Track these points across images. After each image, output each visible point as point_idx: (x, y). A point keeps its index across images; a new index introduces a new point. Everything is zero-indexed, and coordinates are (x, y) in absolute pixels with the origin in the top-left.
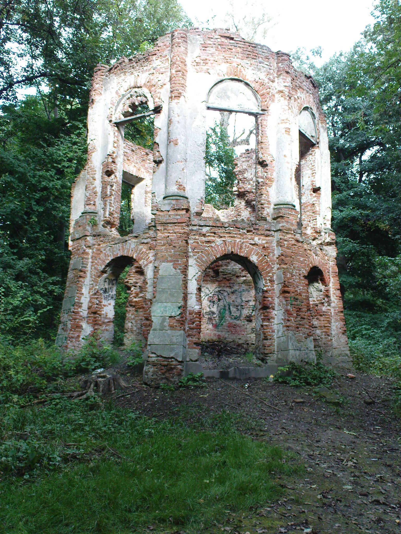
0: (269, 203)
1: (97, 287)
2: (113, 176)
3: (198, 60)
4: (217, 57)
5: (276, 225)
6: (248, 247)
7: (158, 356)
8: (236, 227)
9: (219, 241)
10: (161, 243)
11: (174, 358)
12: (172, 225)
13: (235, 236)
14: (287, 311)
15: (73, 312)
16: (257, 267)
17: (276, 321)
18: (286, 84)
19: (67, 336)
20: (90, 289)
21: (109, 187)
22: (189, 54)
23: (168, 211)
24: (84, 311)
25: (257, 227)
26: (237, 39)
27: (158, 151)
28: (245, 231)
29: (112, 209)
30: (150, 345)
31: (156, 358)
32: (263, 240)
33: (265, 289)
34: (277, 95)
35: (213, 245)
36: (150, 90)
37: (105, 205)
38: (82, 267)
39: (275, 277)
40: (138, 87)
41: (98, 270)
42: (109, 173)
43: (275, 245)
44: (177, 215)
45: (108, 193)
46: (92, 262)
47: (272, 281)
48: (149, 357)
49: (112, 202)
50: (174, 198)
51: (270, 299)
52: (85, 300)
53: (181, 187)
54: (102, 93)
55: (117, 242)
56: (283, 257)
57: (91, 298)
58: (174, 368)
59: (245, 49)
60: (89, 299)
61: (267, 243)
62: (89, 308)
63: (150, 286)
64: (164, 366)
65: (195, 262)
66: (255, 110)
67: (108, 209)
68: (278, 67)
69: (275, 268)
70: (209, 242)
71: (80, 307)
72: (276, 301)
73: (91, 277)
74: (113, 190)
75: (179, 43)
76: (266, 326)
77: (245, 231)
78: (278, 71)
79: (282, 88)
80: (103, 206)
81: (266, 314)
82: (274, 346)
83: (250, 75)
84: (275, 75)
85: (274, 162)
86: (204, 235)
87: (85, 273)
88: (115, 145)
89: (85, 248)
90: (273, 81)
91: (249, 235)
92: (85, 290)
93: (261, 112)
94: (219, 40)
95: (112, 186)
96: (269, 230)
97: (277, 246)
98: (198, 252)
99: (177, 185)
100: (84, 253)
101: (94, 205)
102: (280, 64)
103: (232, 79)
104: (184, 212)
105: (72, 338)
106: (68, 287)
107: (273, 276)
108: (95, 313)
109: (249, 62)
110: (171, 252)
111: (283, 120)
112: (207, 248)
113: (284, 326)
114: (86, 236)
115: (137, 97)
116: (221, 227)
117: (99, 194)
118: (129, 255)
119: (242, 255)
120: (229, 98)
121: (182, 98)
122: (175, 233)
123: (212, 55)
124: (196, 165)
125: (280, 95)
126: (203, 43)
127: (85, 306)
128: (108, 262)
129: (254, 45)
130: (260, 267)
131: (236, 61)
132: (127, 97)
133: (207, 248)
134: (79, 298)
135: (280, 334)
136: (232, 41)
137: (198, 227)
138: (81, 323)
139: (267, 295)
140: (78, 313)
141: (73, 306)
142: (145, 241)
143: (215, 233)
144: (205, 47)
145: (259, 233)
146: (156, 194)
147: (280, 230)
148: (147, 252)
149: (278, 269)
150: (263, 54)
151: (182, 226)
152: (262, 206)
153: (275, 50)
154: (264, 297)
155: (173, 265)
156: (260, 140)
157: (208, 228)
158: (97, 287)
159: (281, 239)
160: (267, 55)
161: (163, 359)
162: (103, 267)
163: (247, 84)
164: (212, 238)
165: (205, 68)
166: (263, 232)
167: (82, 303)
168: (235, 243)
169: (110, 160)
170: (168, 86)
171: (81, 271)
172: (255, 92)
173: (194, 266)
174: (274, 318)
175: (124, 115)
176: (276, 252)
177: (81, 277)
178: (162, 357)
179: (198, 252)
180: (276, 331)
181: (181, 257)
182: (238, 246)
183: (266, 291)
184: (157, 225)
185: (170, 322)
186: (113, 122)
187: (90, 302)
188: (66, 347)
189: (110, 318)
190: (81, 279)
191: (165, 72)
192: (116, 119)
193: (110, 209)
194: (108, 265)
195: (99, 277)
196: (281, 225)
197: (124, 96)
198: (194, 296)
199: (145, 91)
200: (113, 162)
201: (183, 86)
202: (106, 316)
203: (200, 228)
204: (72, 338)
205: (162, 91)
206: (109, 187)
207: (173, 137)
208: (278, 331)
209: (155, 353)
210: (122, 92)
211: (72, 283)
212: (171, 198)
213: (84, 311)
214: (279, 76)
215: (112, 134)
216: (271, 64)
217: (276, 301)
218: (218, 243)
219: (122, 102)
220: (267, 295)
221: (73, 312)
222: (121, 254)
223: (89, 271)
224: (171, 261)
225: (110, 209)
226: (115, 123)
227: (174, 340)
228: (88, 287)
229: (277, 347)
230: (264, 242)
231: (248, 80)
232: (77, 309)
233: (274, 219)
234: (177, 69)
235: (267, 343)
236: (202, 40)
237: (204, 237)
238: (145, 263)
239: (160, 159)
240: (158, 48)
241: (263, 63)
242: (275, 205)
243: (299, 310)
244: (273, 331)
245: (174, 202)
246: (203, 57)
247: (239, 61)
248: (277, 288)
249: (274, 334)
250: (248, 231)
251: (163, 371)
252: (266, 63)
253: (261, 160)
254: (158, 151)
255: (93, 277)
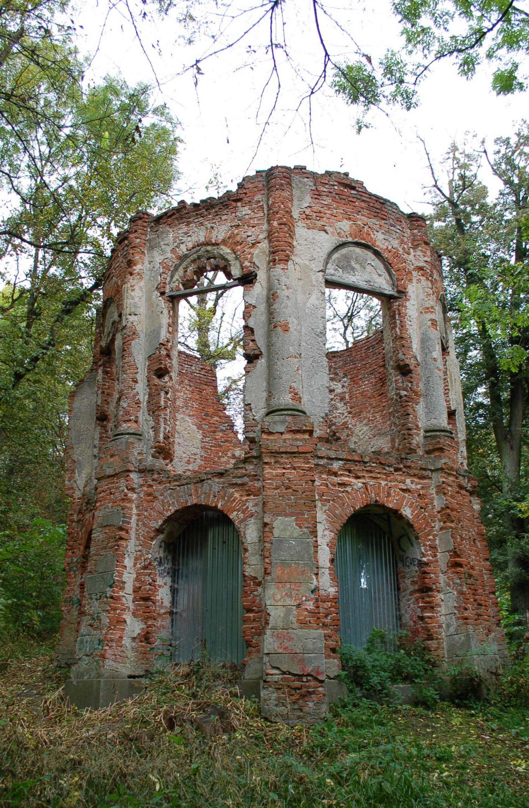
0: (418, 428)
1: (150, 556)
2: (167, 378)
3: (308, 211)
4: (335, 211)
5: (434, 461)
6: (398, 495)
7: (284, 673)
8: (380, 463)
9: (358, 484)
10: (272, 484)
11: (312, 676)
12: (288, 455)
13: (379, 476)
14: (461, 593)
15: (112, 597)
16: (411, 526)
17: (443, 610)
18: (426, 259)
19: (102, 637)
20: (136, 559)
21: (163, 394)
22: (295, 202)
23: (282, 434)
24: (127, 596)
25: (408, 464)
26: (360, 190)
27: (253, 341)
28: (392, 469)
29: (168, 429)
30: (268, 654)
31: (280, 676)
32: (417, 484)
33: (425, 559)
34: (415, 273)
35: (349, 489)
36: (233, 250)
37: (158, 423)
38: (124, 522)
39: (437, 542)
40: (213, 245)
41: (150, 528)
42: (161, 373)
43: (434, 492)
44: (297, 440)
45: (162, 403)
46: (138, 515)
47: (433, 548)
48: (267, 674)
49: (168, 418)
50: (290, 412)
51: (432, 575)
52: (129, 578)
53: (297, 397)
54: (146, 252)
55: (184, 482)
56: (448, 511)
57: (138, 574)
58: (314, 692)
59: (372, 205)
60: (135, 576)
61: (423, 488)
62: (136, 590)
63: (252, 555)
64: (296, 689)
65: (325, 516)
66: (388, 290)
67: (162, 429)
68: (413, 234)
69: (437, 528)
70: (340, 485)
71: (123, 588)
72: (441, 578)
73: (138, 539)
74: (168, 399)
75: (282, 185)
76: (430, 617)
77: (392, 469)
78: (414, 240)
79: (422, 264)
80: (152, 423)
81: (428, 599)
82: (443, 648)
83: (380, 240)
84: (410, 245)
85: (419, 368)
86: (335, 474)
87: (127, 532)
88: (171, 329)
89: (126, 491)
90: (409, 254)
91: (398, 476)
92: (128, 562)
93: (396, 294)
94: (336, 187)
95: (167, 393)
96: (425, 469)
97: (437, 493)
98: (328, 501)
99: (290, 393)
100: (126, 499)
101: (136, 422)
102: (415, 231)
103: (358, 244)
104: (307, 436)
105: (112, 640)
106: (95, 555)
107: (435, 540)
108: (146, 599)
109: (377, 223)
110: (289, 499)
111: (428, 308)
112: (340, 495)
113: (458, 618)
114: (129, 471)
115: (209, 259)
116: (359, 462)
117: (144, 405)
118: (209, 503)
119: (390, 506)
120: (353, 269)
121: (290, 263)
122: (294, 468)
123: (328, 206)
124: (315, 364)
125: (420, 274)
126: (314, 188)
127: (129, 588)
128: (169, 514)
129: (382, 201)
130: (416, 525)
131: (362, 219)
132: (192, 258)
133: (340, 495)
134: (121, 575)
135: (452, 630)
136: (353, 192)
137: (326, 461)
138: (124, 616)
139: (427, 569)
140: (118, 599)
141: (111, 587)
142: (239, 481)
143: (350, 471)
144: (317, 195)
145: (411, 472)
146: (252, 406)
147: (442, 469)
148: (244, 499)
149: (441, 529)
150: (393, 214)
151: (305, 458)
152: (410, 432)
153: (407, 211)
154: (425, 572)
155: (296, 520)
156: (399, 334)
157: (340, 462)
158: (150, 556)
159: (443, 482)
160: (398, 216)
161: (293, 678)
162: (160, 522)
163: (377, 254)
164: (347, 479)
165: (319, 223)
166: (416, 472)
167: (124, 583)
168: (379, 487)
169: (164, 352)
170: (265, 245)
171: (121, 529)
172: (388, 265)
173: (324, 522)
174: (440, 606)
175: (184, 285)
176: (435, 503)
177: (121, 538)
178: (290, 673)
179: (328, 501)
180: (444, 625)
181: (307, 508)
182: (384, 492)
183: (426, 564)
184: (263, 455)
185: (298, 615)
186: (166, 295)
187: (137, 579)
188: (103, 657)
189: (166, 607)
190: (122, 542)
191: (258, 225)
192: (172, 290)
193: (165, 429)
194: (168, 520)
195: (152, 539)
196: (443, 461)
197: (186, 256)
198: (327, 571)
199: (225, 250)
200: (168, 356)
201: (291, 246)
202: (162, 603)
203: (330, 462)
204: (112, 640)
205: (256, 251)
206: (163, 394)
207: (280, 319)
208: (448, 626)
209: (278, 668)
210: (183, 249)
211: (105, 548)
212: (286, 412)
213: (127, 596)
214: (415, 247)
215: (166, 312)
216: (404, 230)
217: (442, 578)
218: (355, 487)
219: (184, 265)
220: (427, 569)
221: (112, 597)
222: (195, 502)
223: (134, 530)
224: (291, 515)
225: (165, 429)
226: (170, 296)
227: (310, 646)
228: (133, 556)
229: (449, 651)
230: (419, 486)
231: (378, 246)
232: (118, 592)
233: (428, 452)
234: (281, 221)
235: (433, 644)
236: (311, 184)
237: (336, 477)
238: (241, 516)
239: (257, 352)
240: (245, 191)
241: (395, 226)
242: (426, 431)
243: (475, 592)
244: (440, 626)
245: (289, 419)
246: (317, 208)
247: (365, 219)
248: (443, 559)
249: (441, 630)
250: (397, 470)
251: (293, 698)
252: (398, 227)
253: (402, 363)
254: (253, 341)
255: (142, 538)
